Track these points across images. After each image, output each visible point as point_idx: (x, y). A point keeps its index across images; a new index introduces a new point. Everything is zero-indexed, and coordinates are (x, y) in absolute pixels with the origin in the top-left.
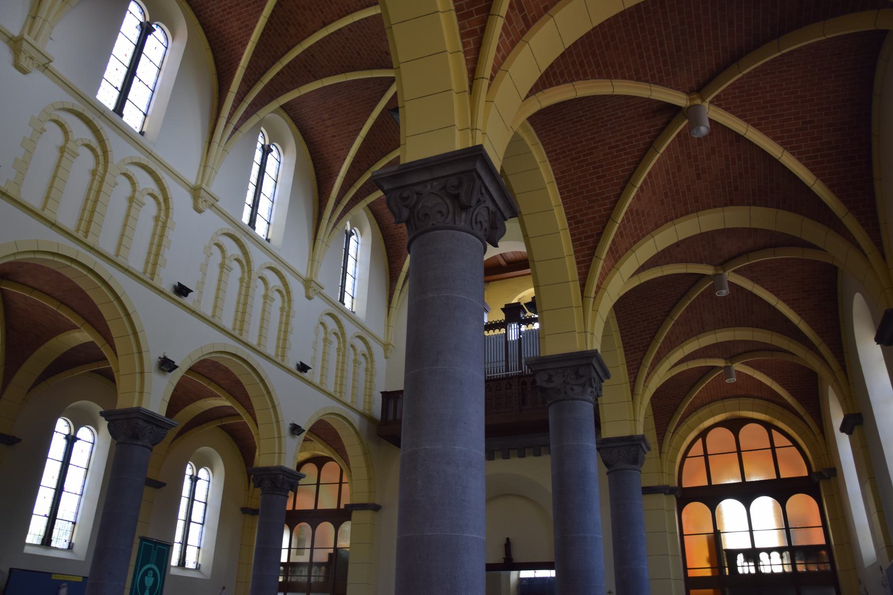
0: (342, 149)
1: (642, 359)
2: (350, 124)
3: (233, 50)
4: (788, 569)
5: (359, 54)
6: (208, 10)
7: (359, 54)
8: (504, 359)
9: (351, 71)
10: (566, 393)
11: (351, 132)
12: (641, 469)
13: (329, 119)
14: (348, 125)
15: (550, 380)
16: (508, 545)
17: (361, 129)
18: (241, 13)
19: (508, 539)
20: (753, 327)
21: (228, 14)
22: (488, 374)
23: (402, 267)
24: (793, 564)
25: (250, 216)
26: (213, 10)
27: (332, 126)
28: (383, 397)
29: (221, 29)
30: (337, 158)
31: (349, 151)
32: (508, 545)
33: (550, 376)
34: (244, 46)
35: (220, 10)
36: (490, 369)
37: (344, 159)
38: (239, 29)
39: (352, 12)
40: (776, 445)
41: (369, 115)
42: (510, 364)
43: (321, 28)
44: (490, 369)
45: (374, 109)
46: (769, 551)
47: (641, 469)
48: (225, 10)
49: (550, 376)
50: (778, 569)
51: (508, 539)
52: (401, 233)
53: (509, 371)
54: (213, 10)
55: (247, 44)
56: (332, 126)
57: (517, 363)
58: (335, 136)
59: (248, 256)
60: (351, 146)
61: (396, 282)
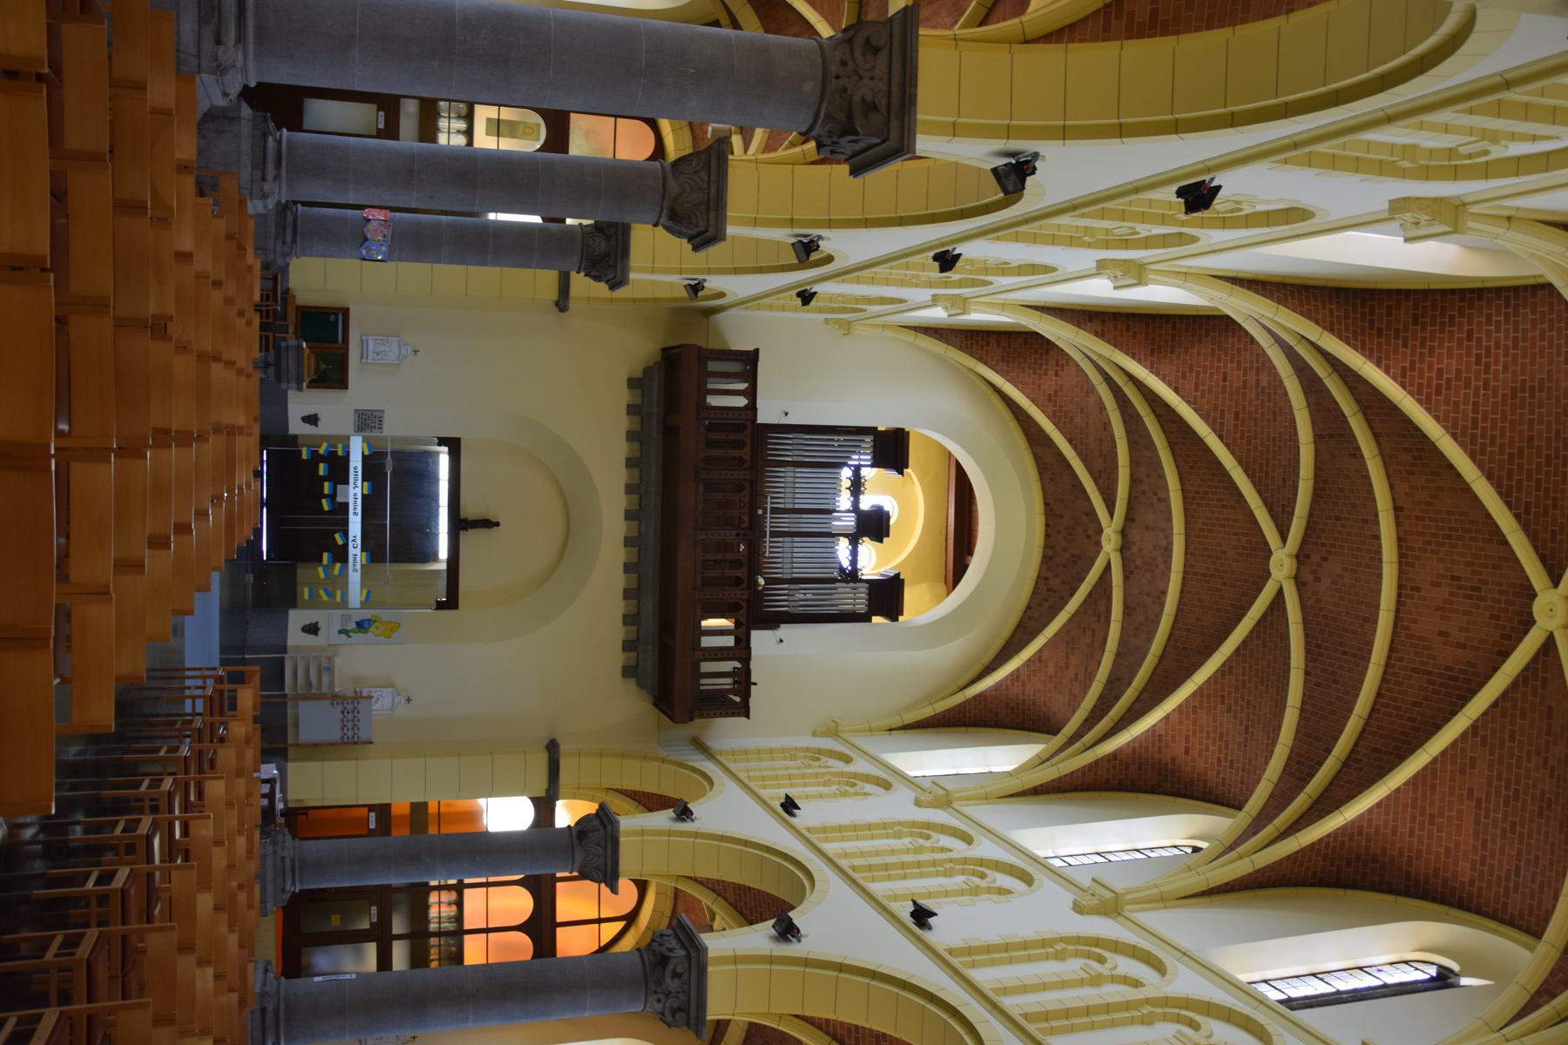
0: (1196, 389)
1: (725, 899)
2: (1236, 418)
3: (1405, 345)
4: (433, 927)
5: (1337, 518)
6: (1502, 318)
7: (1337, 518)
8: (797, 506)
9: (1315, 489)
10: (655, 992)
11: (1222, 416)
12: (660, 227)
13: (1258, 382)
14: (1237, 413)
15: (675, 975)
16: (488, 524)
17: (1221, 437)
18: (1467, 386)
19: (497, 524)
20: (748, 1031)
21: (1478, 357)
22: (772, 498)
23: (986, 363)
24: (439, 934)
25: (903, 978)
26: (1498, 330)
27: (1245, 381)
28: (747, 352)
29: (1466, 304)
30: (1184, 373)
31: (1188, 402)
32: (488, 524)
33: (680, 976)
34: (1402, 379)
35: (1492, 344)
36: (783, 480)
37: (1176, 390)
38: (1440, 371)
39: (1400, 564)
40: (603, 925)
41: (1240, 461)
42: (781, 539)
43: (1394, 500)
44: (783, 480)
45: (1248, 475)
46: (460, 904)
47: (660, 227)
48: (1488, 355)
49: (680, 976)
50: (433, 912)
51: (497, 524)
52: (1046, 370)
53: (771, 537)
54: (1498, 330)
55: (1403, 385)
56: (1245, 381)
57: (780, 576)
58: (1224, 380)
59: (1055, 138)
60: (1195, 410)
61: (961, 349)
